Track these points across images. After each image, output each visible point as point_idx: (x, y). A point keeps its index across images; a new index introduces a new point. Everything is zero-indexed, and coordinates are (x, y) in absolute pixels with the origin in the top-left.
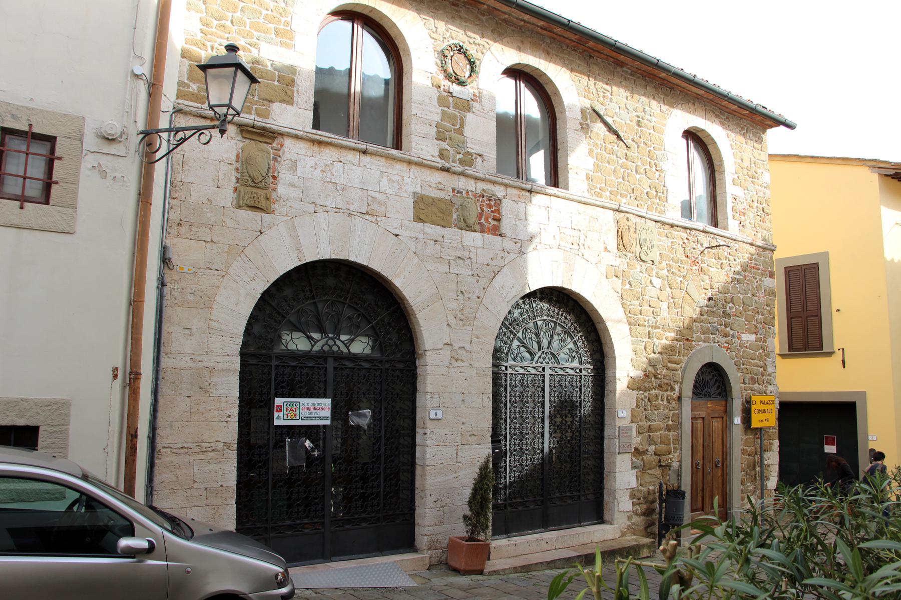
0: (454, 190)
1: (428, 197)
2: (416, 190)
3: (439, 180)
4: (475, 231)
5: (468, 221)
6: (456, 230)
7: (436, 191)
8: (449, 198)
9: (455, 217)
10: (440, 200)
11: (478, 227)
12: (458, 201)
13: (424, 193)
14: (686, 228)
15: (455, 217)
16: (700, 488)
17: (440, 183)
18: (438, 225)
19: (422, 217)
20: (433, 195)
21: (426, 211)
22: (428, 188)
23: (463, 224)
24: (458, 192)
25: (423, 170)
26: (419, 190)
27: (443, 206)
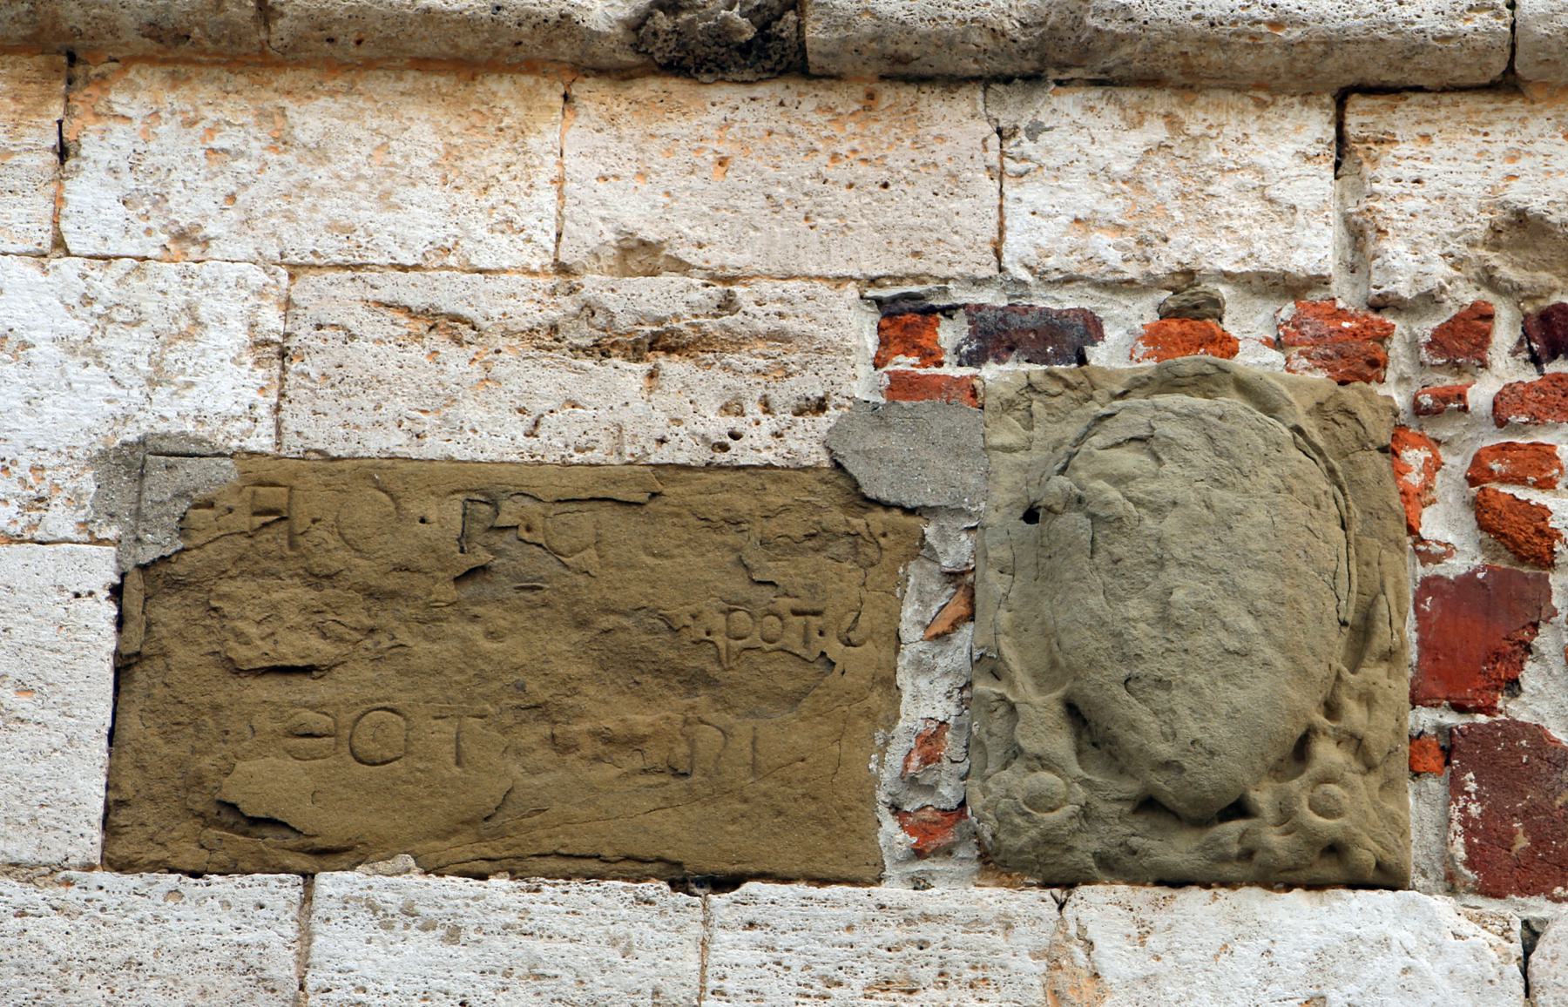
0: (905, 316)
1: (387, 479)
2: (169, 414)
3: (638, 212)
4: (1333, 866)
5: (1144, 725)
6: (958, 894)
7: (549, 380)
8: (806, 443)
9: (925, 700)
10: (641, 494)
11: (1424, 816)
12: (978, 457)
13: (320, 428)
14: (311, 735)
15: (925, 700)
16: (638, 867)
17: (639, 255)
18: (631, 866)
19: (267, 779)
20: (489, 435)
21: (353, 683)
22: (380, 350)
23: (1062, 782)
24: (995, 336)
25: (314, 117)
26: (222, 398)
27: (692, 576)
